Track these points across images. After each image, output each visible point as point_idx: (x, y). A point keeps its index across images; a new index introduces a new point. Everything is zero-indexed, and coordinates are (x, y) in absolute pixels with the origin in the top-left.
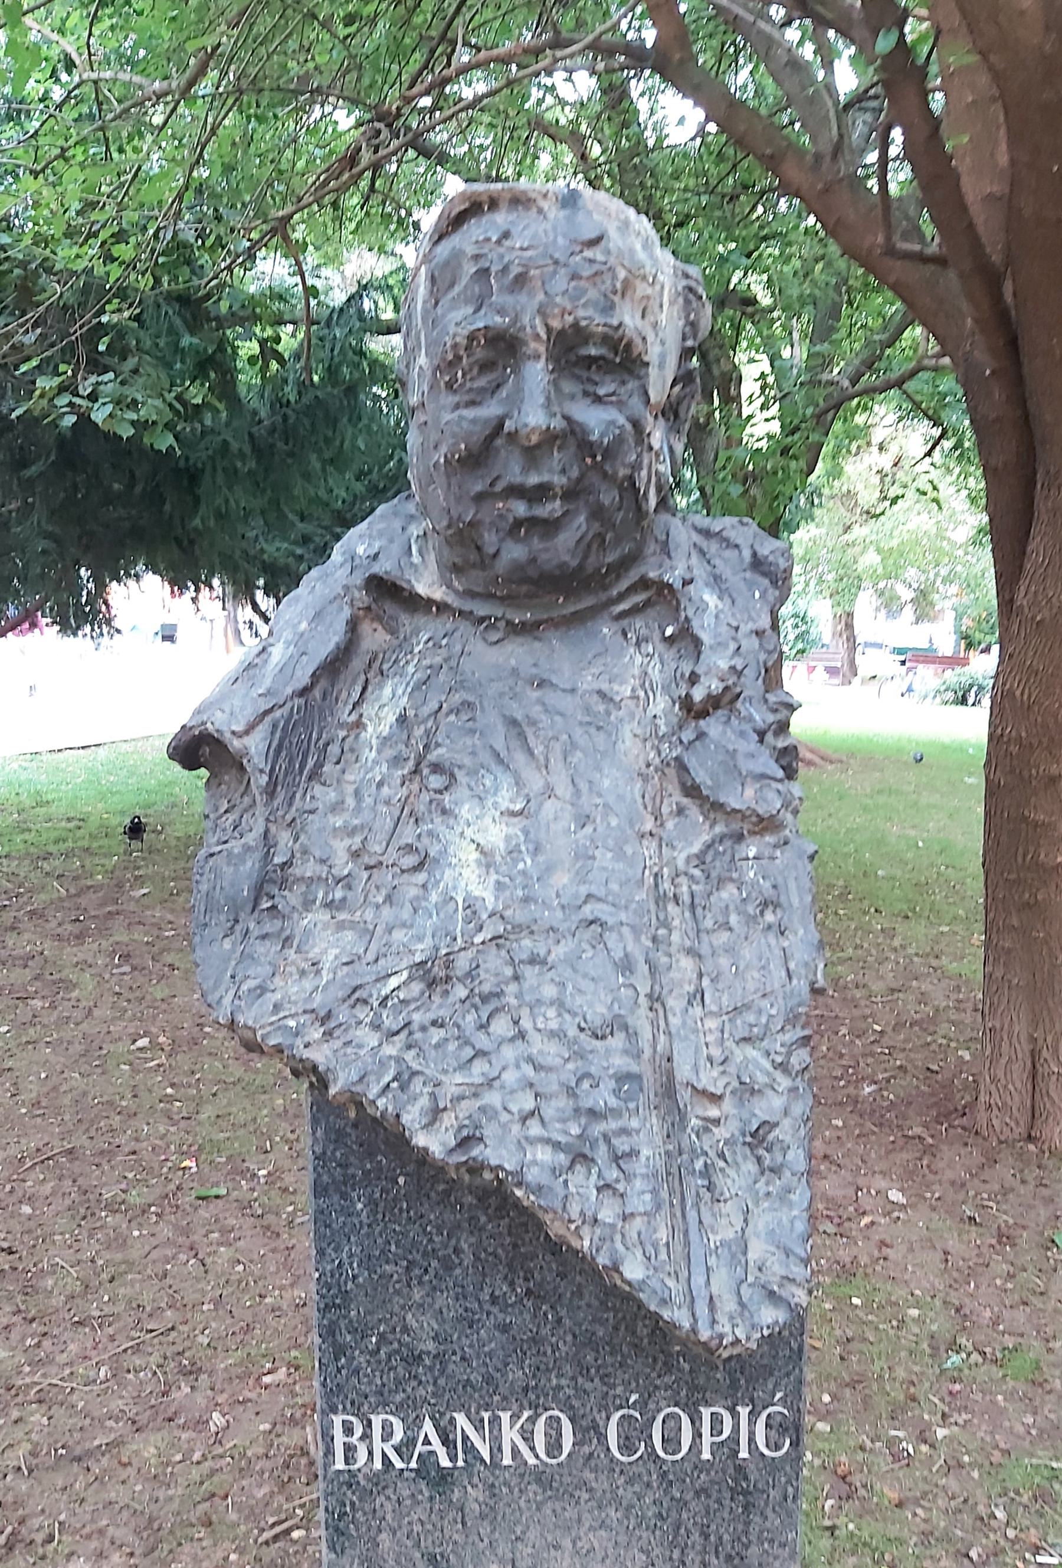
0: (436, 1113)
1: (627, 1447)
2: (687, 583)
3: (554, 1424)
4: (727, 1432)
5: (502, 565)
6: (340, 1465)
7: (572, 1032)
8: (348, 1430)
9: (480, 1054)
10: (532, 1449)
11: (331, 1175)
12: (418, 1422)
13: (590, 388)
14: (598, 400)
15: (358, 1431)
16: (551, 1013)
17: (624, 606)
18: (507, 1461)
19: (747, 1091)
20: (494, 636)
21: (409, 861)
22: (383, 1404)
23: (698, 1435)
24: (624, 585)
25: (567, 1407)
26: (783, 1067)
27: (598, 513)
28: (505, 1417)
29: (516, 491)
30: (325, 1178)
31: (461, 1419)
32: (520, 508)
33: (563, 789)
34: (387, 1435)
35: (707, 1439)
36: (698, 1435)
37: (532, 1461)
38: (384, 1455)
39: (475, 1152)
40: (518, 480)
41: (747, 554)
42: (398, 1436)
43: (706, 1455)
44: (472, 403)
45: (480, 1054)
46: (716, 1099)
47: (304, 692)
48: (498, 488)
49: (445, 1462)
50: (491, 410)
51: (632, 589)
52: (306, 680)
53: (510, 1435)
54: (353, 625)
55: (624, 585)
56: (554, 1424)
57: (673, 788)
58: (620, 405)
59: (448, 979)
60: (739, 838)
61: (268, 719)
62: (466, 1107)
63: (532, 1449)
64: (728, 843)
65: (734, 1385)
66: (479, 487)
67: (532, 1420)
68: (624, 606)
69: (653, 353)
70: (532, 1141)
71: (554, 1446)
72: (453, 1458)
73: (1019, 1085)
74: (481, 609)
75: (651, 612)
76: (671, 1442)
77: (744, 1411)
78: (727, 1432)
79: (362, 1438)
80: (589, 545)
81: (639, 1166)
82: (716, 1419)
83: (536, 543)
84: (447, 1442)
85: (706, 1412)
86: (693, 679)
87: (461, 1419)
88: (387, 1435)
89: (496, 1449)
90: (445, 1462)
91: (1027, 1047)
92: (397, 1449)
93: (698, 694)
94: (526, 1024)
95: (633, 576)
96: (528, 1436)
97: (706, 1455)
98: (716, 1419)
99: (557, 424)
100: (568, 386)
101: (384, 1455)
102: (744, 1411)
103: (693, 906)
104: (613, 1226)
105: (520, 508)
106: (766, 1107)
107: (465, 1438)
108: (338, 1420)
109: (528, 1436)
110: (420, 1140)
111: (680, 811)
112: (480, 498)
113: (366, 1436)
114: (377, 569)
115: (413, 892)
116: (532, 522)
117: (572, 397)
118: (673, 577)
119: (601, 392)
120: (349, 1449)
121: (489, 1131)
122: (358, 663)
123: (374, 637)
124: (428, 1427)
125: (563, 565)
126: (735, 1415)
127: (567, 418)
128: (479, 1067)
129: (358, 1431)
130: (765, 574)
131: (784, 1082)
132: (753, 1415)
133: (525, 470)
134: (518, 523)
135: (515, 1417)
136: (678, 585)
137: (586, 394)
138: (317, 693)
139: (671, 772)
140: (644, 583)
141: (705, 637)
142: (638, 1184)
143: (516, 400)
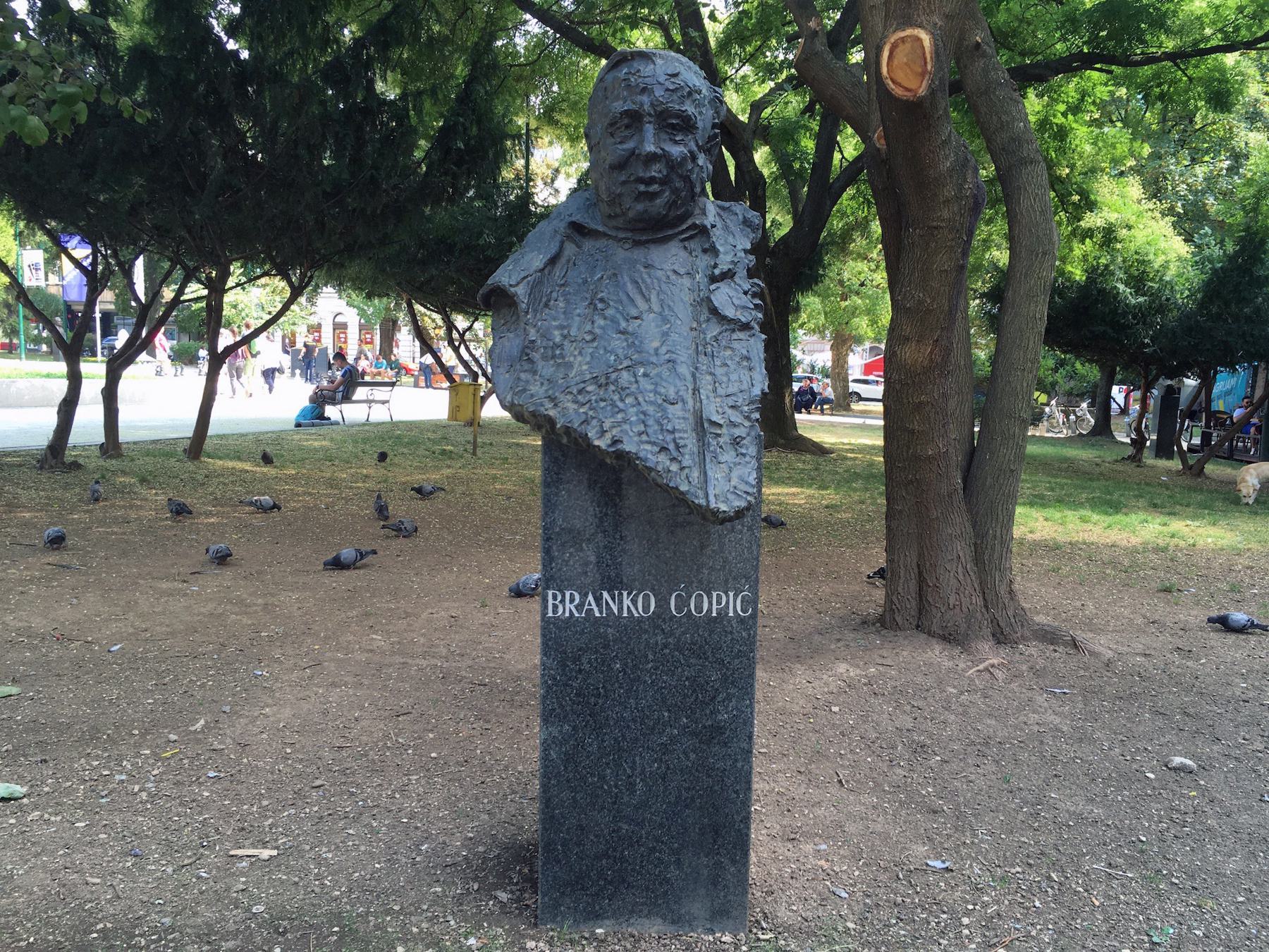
0: (603, 433)
1: (678, 609)
2: (713, 226)
3: (646, 598)
4: (724, 603)
5: (631, 214)
6: (550, 614)
7: (660, 401)
8: (555, 597)
9: (621, 411)
10: (637, 609)
11: (551, 477)
12: (586, 595)
13: (672, 137)
14: (676, 142)
15: (559, 598)
16: (652, 395)
17: (683, 236)
18: (625, 615)
19: (733, 425)
20: (627, 246)
21: (588, 338)
22: (570, 587)
23: (710, 603)
24: (684, 227)
25: (653, 590)
26: (748, 418)
27: (675, 191)
28: (625, 593)
29: (641, 180)
30: (549, 479)
31: (605, 595)
32: (642, 188)
33: (656, 307)
34: (572, 601)
35: (715, 607)
36: (710, 603)
37: (636, 615)
38: (570, 610)
39: (620, 446)
40: (641, 175)
41: (741, 217)
42: (577, 601)
43: (714, 614)
44: (620, 143)
45: (621, 411)
46: (720, 426)
47: (542, 270)
48: (632, 179)
49: (597, 614)
50: (630, 145)
51: (688, 229)
52: (541, 266)
53: (627, 602)
54: (562, 243)
55: (684, 227)
56: (646, 598)
57: (706, 311)
58: (685, 145)
59: (607, 384)
60: (733, 331)
61: (526, 281)
62: (614, 432)
63: (637, 609)
64: (728, 333)
65: (726, 581)
66: (623, 178)
67: (637, 596)
68: (683, 236)
69: (700, 124)
70: (643, 442)
71: (646, 607)
72: (601, 612)
73: (914, 596)
74: (622, 235)
75: (697, 240)
76: (699, 608)
77: (731, 594)
78: (724, 603)
79: (561, 602)
80: (672, 205)
81: (686, 451)
82: (719, 597)
83: (648, 203)
84: (599, 605)
85: (715, 594)
86: (715, 266)
87: (605, 595)
88: (572, 601)
89: (620, 609)
90: (597, 614)
91: (916, 571)
92: (576, 607)
93: (717, 272)
94: (641, 399)
95: (690, 222)
96: (634, 602)
97: (714, 614)
98: (719, 597)
99: (659, 151)
100: (664, 136)
101: (570, 610)
102: (731, 594)
103: (713, 356)
104: (676, 473)
105: (642, 188)
106: (737, 432)
107: (607, 603)
108: (550, 593)
109: (634, 602)
110: (596, 443)
111: (708, 320)
112: (624, 183)
113: (563, 601)
114: (573, 219)
115: (591, 350)
116: (646, 193)
117: (665, 140)
118: (708, 223)
119: (677, 139)
120: (555, 607)
121: (625, 440)
122: (563, 260)
123: (570, 249)
124: (590, 598)
125: (659, 213)
126: (728, 596)
127: (662, 149)
128: (620, 416)
129: (559, 598)
130: (748, 226)
131: (747, 424)
132: (736, 596)
133: (644, 171)
134: (641, 194)
135: (629, 594)
136: (709, 227)
137: (671, 140)
138: (546, 271)
139: (704, 304)
140: (694, 226)
141: (721, 249)
142: (687, 457)
143: (642, 141)
